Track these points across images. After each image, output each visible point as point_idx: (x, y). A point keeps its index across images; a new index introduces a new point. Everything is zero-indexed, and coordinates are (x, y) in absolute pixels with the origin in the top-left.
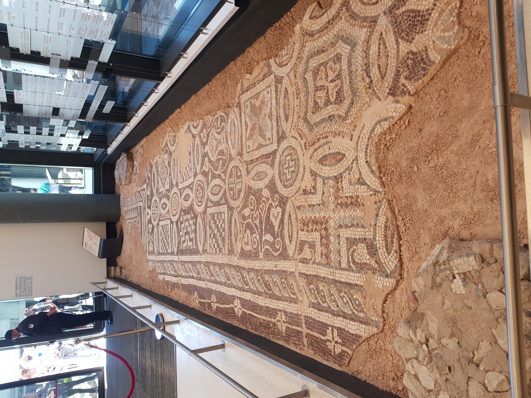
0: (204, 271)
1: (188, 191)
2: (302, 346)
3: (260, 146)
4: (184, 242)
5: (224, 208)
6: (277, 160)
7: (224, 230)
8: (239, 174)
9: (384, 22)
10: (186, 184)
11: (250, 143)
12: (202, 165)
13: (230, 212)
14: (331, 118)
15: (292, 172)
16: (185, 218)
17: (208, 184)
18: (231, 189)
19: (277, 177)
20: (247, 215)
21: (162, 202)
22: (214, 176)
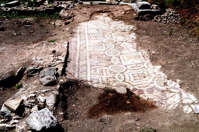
0: (83, 42)
1: (110, 36)
2: (123, 107)
3: (124, 60)
4: (92, 35)
5: (104, 49)
6: (119, 65)
7: (97, 49)
8: (116, 54)
9: (152, 85)
10: (113, 36)
11: (125, 57)
12: (119, 41)
13: (103, 51)
14: (130, 78)
15: (116, 70)
16: (101, 36)
17: (113, 43)
18: (111, 51)
19: (115, 65)
20: (103, 56)
21: (106, 37)
22: (115, 46)
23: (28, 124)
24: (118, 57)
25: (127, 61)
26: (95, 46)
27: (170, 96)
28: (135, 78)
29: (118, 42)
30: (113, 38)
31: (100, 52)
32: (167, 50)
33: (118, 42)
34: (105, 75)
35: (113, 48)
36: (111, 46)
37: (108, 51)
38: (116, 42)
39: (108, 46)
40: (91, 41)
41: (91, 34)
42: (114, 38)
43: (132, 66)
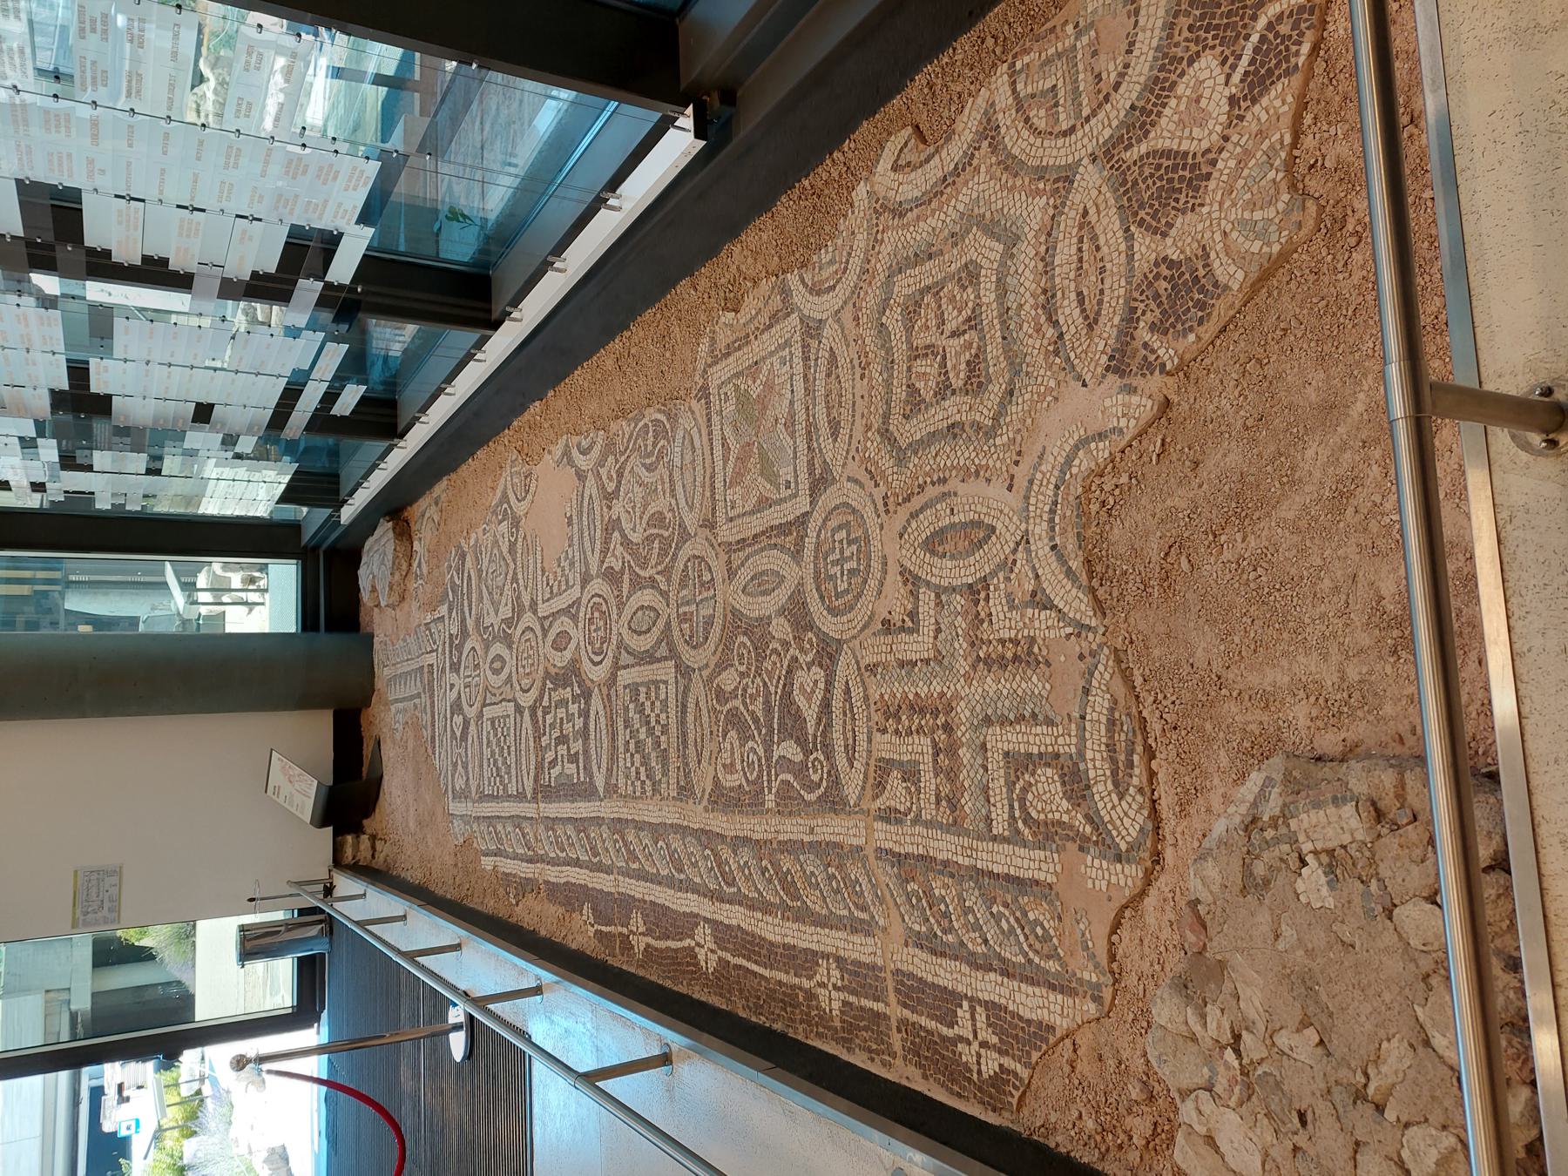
1: (564, 623)
3: (764, 503)
4: (553, 763)
6: (809, 542)
8: (706, 577)
11: (735, 494)
12: (605, 552)
14: (954, 430)
16: (556, 696)
17: (621, 606)
18: (685, 618)
19: (810, 585)
22: (637, 584)
23: (1320, 1050)
24: (737, 558)
25: (772, 478)
26: (651, 731)
27: (214, 476)
28: (957, 383)
29: (611, 561)
30: (577, 602)
31: (691, 706)
32: (980, 385)
33: (611, 561)
34: (937, 687)
35: (660, 605)
36: (643, 620)
37: (682, 648)
38: (612, 577)
39: (643, 643)
40: (600, 782)
41: (539, 767)
42: (575, 592)
43: (824, 429)
